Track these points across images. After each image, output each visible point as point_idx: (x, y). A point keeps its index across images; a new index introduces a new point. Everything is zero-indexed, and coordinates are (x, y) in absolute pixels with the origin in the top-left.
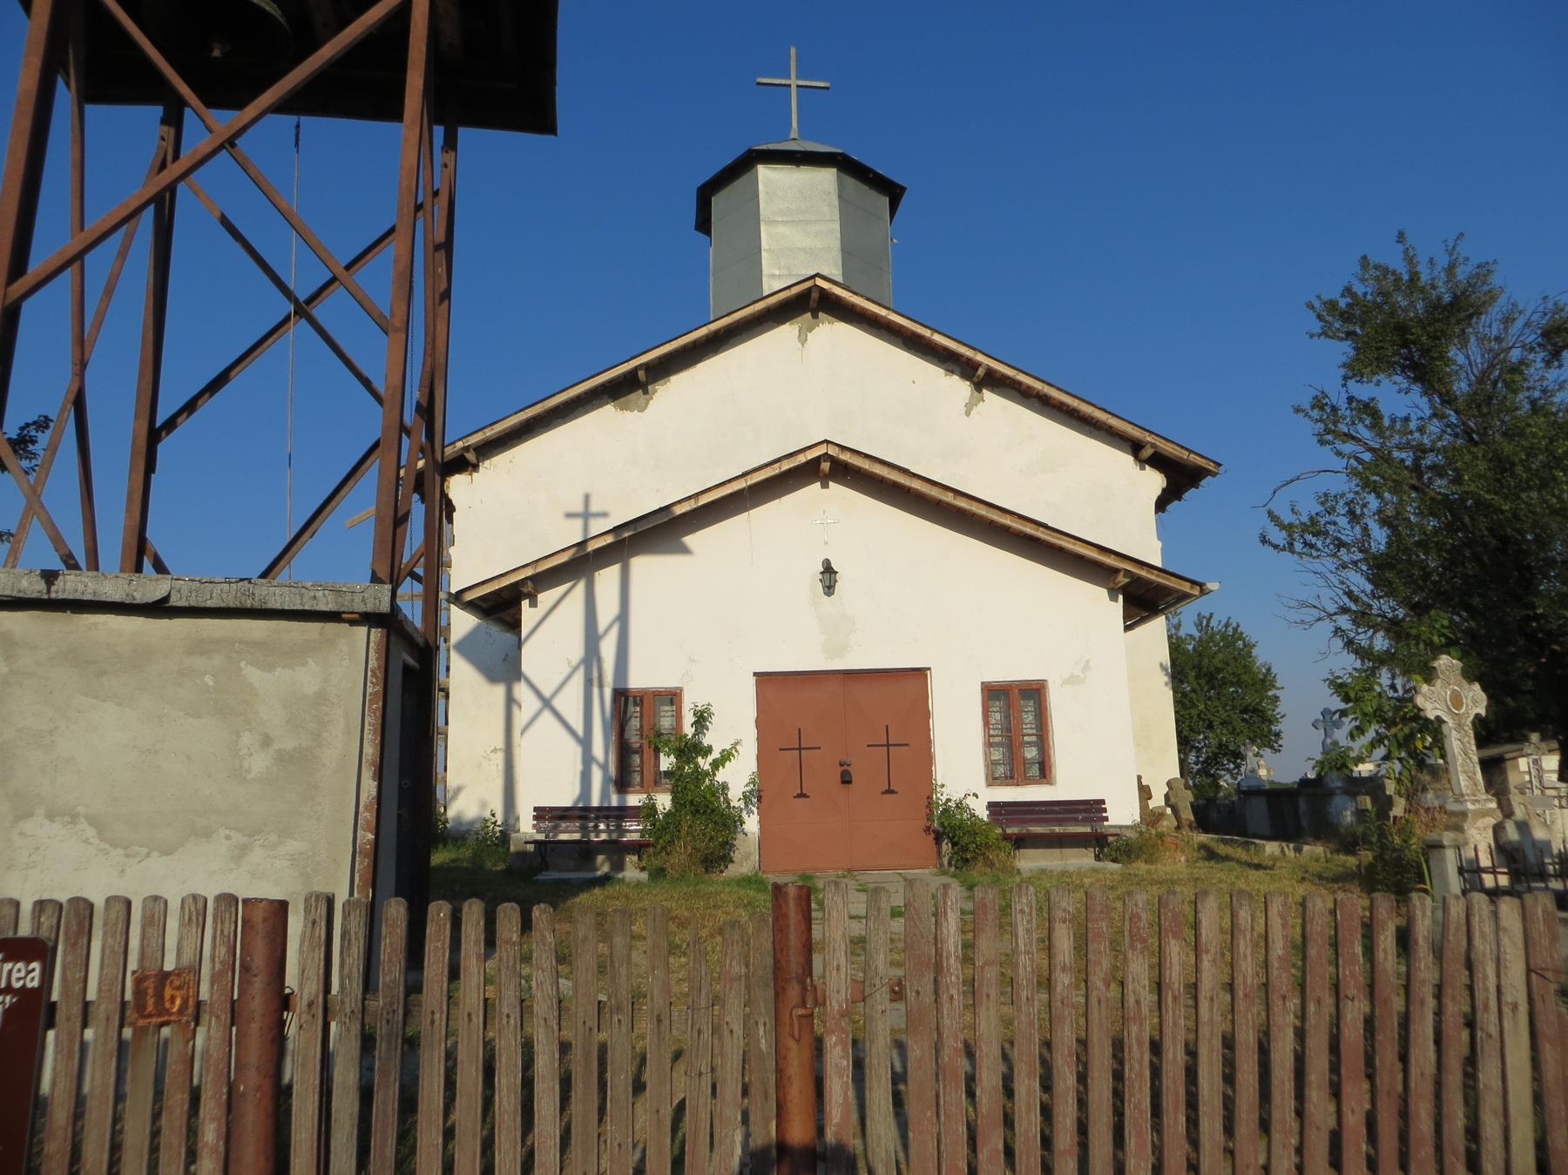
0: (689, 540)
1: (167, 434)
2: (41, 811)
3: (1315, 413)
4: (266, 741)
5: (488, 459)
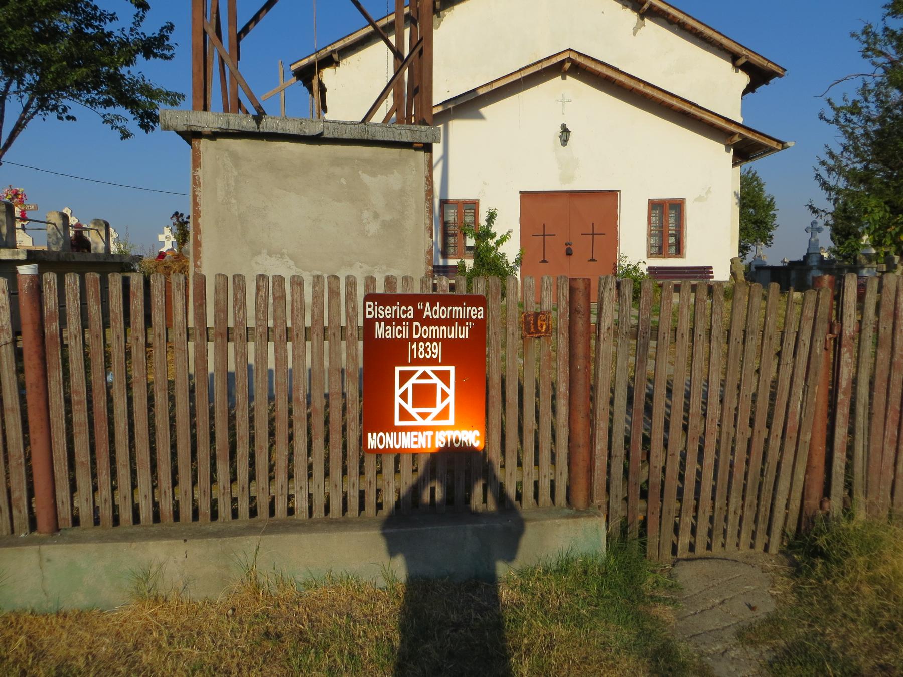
0: (484, 111)
1: (245, 36)
2: (265, 251)
3: (864, 38)
4: (376, 216)
5: (345, 58)
